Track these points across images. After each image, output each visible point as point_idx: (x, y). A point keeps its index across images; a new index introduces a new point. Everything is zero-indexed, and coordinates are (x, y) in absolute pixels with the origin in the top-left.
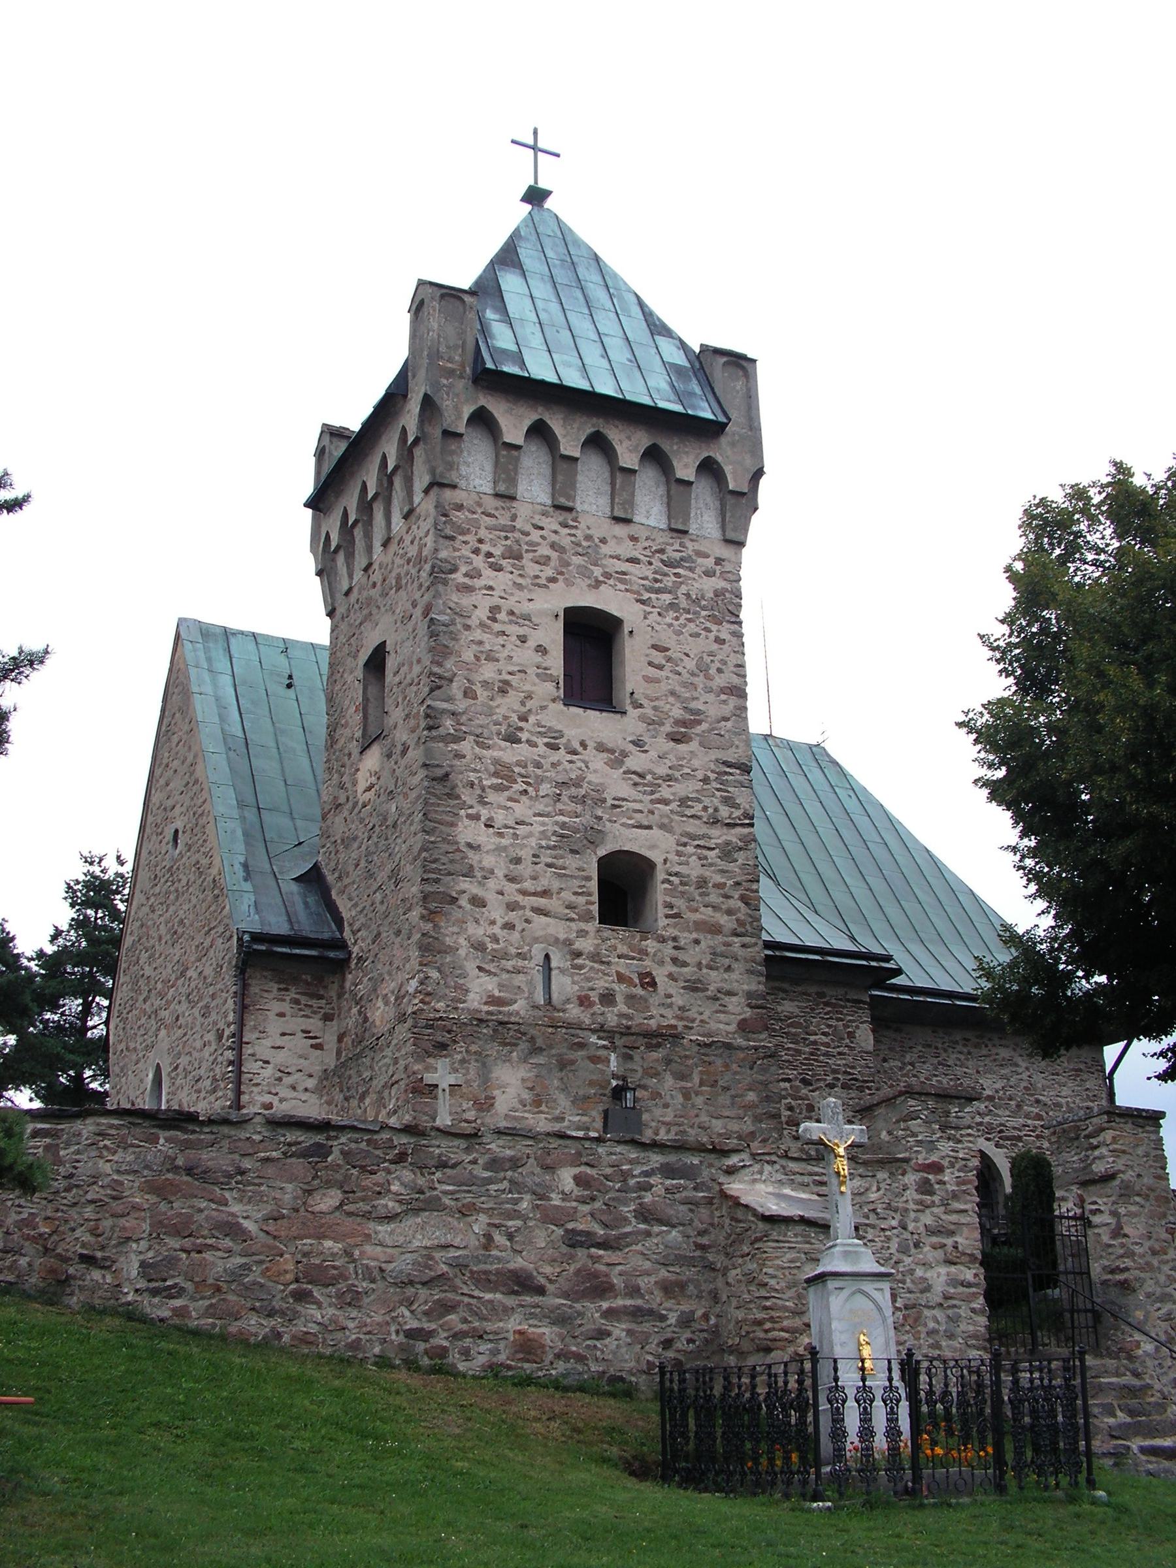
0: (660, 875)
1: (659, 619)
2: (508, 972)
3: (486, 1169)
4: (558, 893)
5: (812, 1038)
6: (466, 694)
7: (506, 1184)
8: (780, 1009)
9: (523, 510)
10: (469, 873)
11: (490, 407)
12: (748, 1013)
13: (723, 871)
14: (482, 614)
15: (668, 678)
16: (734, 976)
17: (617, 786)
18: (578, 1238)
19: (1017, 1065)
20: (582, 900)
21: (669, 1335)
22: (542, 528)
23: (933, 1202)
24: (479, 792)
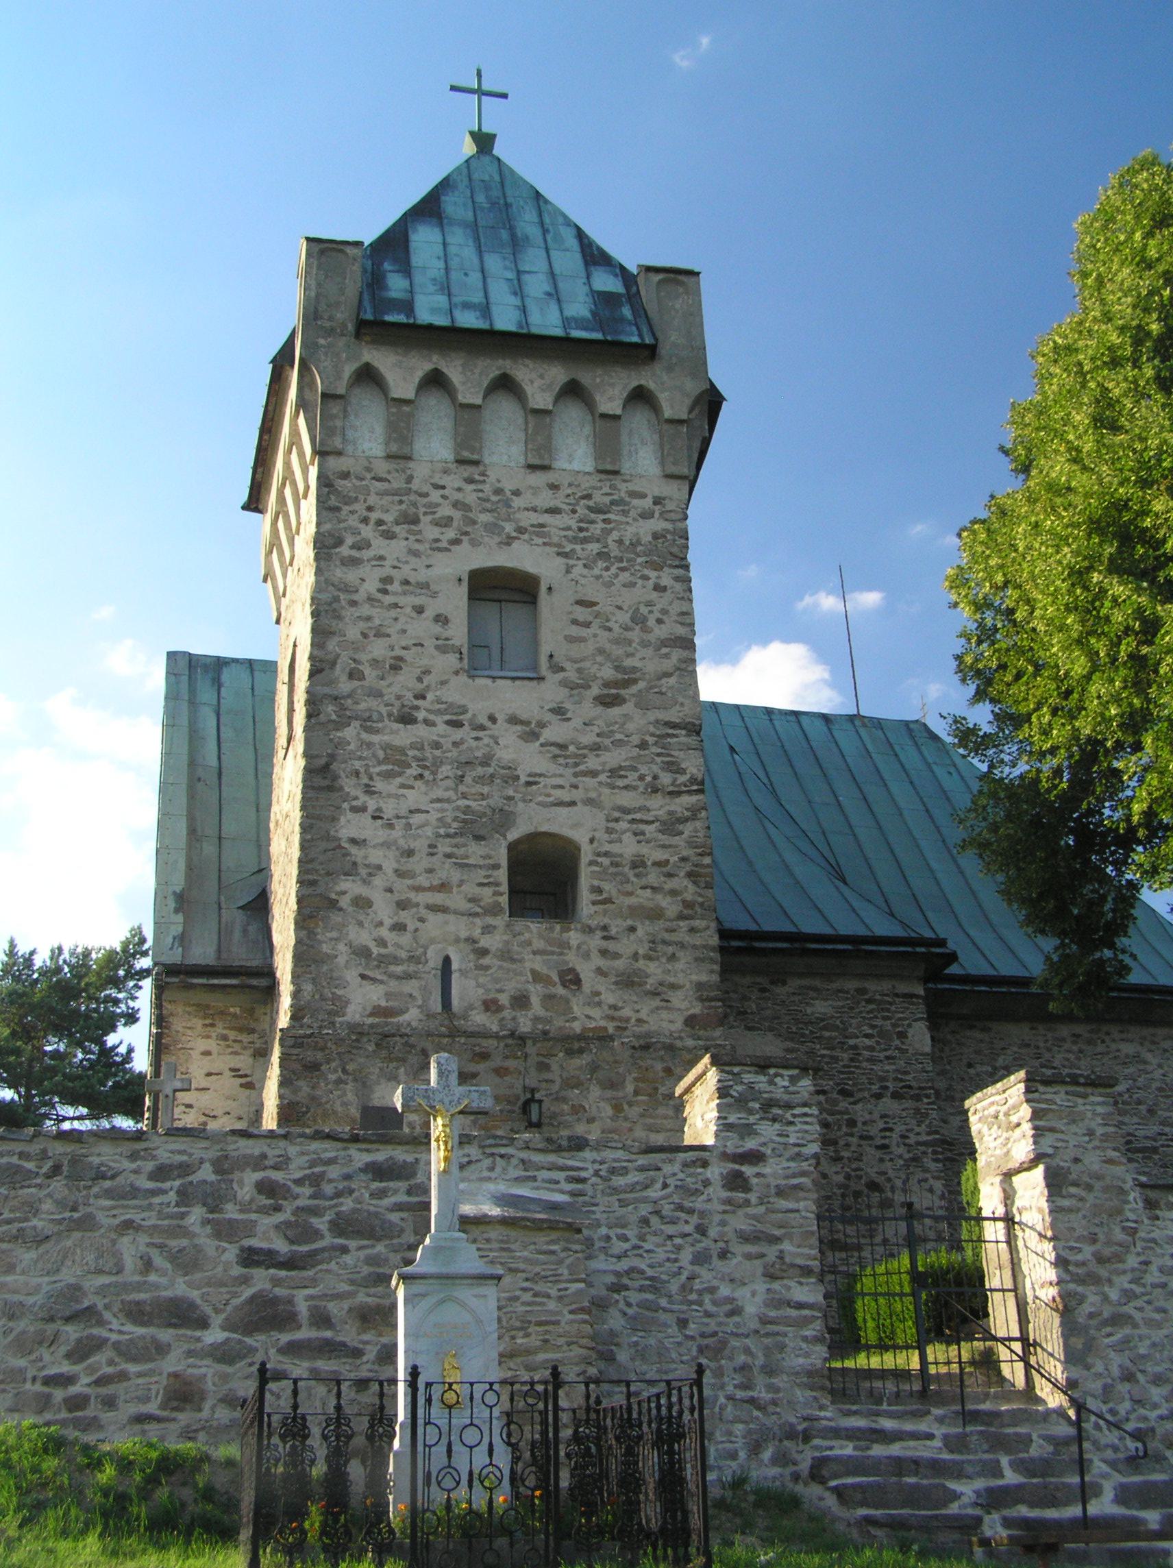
0: (585, 859)
1: (585, 571)
4: (459, 886)
5: (852, 1042)
6: (351, 676)
8: (809, 1010)
9: (420, 470)
10: (352, 870)
11: (376, 364)
12: (697, 1009)
13: (664, 846)
14: (371, 586)
15: (595, 636)
16: (680, 965)
17: (531, 759)
19: (1145, 1062)
20: (487, 891)
22: (443, 487)
24: (365, 780)
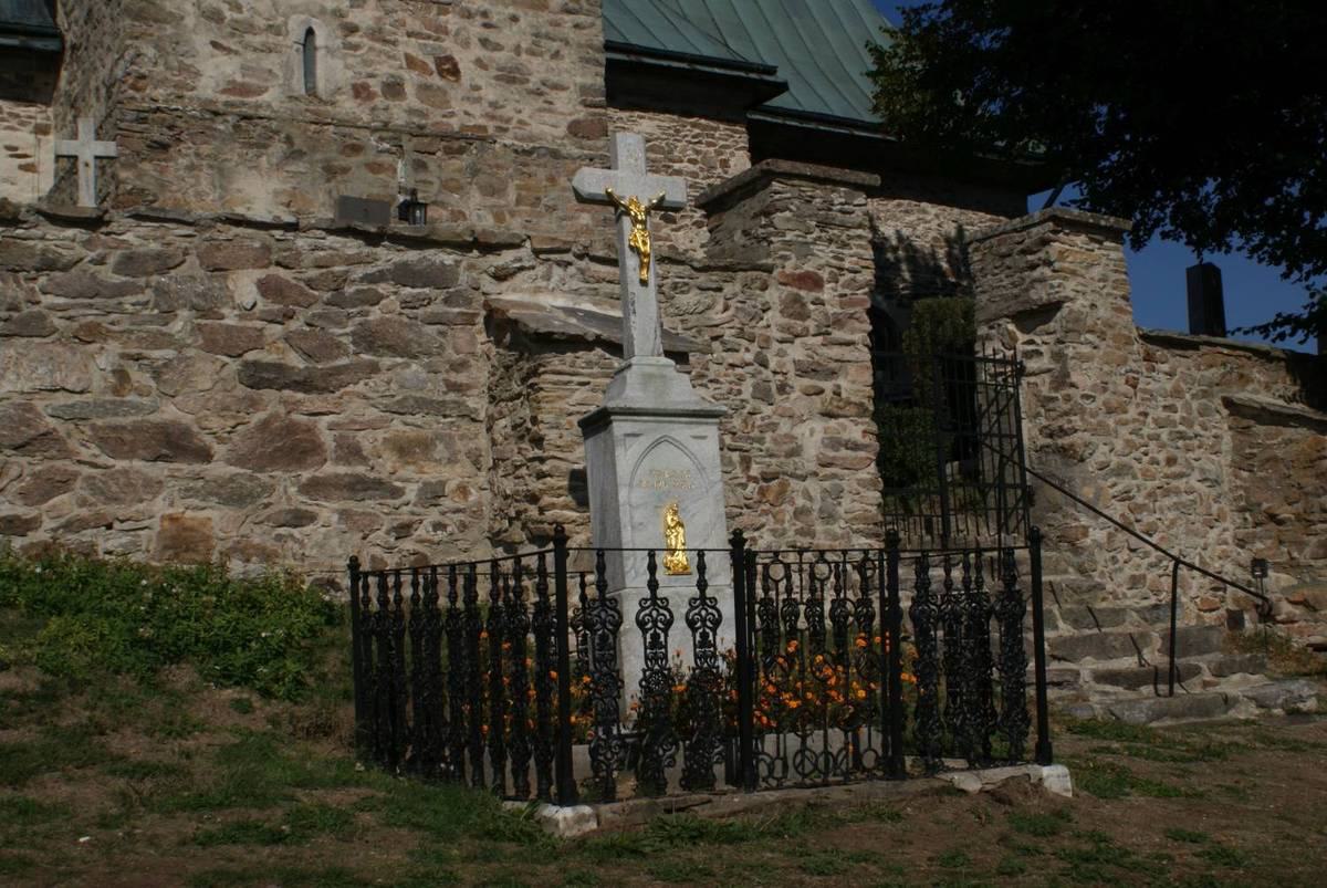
2: (255, 50)
3: (117, 271)
5: (677, 166)
7: (149, 295)
12: (582, 113)
16: (565, 64)
18: (265, 375)
19: (925, 212)
21: (406, 518)
23: (807, 329)
